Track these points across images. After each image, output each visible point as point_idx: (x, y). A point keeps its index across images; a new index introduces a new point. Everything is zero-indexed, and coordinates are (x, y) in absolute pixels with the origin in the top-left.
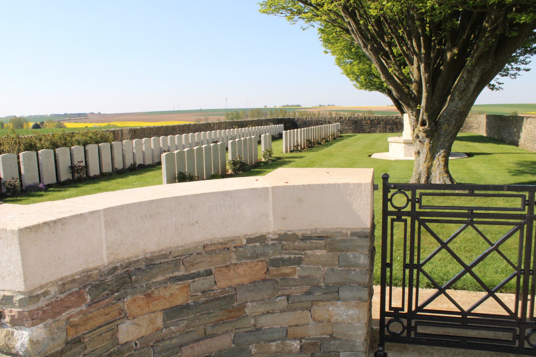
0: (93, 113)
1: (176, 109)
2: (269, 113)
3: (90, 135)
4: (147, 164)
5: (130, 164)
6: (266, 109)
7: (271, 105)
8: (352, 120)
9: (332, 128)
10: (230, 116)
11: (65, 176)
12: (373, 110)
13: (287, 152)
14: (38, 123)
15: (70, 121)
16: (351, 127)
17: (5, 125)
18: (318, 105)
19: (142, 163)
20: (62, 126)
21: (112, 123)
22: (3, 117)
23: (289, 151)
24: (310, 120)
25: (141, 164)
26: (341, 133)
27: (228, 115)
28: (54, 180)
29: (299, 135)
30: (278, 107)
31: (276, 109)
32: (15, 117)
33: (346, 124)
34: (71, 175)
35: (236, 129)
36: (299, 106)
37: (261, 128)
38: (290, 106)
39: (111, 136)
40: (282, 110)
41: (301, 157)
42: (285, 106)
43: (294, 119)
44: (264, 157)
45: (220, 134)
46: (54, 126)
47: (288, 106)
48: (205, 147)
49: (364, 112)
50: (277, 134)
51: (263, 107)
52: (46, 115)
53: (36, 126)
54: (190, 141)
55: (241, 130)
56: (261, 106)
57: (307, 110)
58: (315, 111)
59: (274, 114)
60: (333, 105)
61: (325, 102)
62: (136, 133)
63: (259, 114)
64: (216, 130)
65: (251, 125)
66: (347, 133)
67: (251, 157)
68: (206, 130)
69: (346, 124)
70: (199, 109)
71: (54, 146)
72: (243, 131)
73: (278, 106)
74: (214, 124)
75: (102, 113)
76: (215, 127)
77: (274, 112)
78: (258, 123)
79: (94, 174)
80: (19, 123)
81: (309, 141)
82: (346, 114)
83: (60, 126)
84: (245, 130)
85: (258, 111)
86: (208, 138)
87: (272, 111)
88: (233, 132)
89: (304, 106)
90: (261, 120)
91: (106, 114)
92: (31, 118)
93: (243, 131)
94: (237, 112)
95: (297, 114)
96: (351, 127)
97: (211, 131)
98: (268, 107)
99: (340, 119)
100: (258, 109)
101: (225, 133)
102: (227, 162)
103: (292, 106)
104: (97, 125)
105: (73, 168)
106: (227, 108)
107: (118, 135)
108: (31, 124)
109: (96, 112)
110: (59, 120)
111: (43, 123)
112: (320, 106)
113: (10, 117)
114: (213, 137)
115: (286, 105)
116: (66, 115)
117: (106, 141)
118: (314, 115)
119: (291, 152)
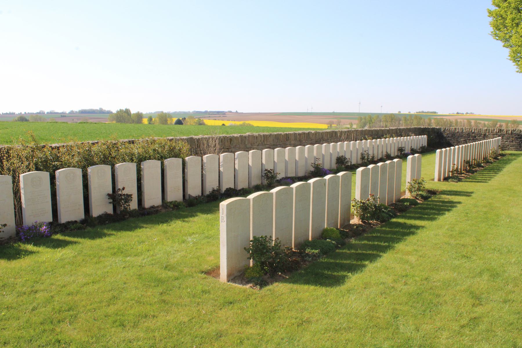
0: (231, 112)
1: (310, 111)
2: (403, 119)
3: (156, 146)
4: (239, 187)
5: (211, 190)
6: (400, 114)
7: (405, 110)
8: (516, 134)
9: (492, 144)
10: (363, 120)
11: (100, 207)
12: (518, 120)
13: (439, 180)
14: (181, 119)
15: (209, 118)
16: (514, 143)
17: (153, 119)
18: (456, 113)
19: (233, 187)
20: (201, 122)
21: (247, 122)
22: (153, 112)
23: (442, 178)
24: (460, 131)
25: (230, 189)
26: (503, 150)
27: (361, 119)
28: (79, 215)
29: (454, 155)
30: (412, 113)
31: (411, 116)
32: (162, 112)
33: (508, 139)
34: (111, 207)
35: (369, 141)
36: (435, 113)
37: (400, 139)
38: (425, 113)
39: (186, 148)
40: (418, 117)
41: (468, 194)
42: (420, 112)
43: (440, 129)
44: (411, 191)
45: (348, 146)
46: (194, 122)
47: (423, 112)
48: (314, 183)
49: (507, 122)
50: (418, 148)
51: (397, 113)
52: (189, 112)
53: (179, 122)
54: (306, 155)
55: (376, 142)
56: (395, 111)
57: (444, 117)
58: (452, 119)
59: (408, 120)
60: (472, 113)
61: (463, 110)
62: (230, 144)
63: (392, 119)
64: (343, 141)
65: (388, 136)
66: (508, 150)
67: (390, 192)
68: (328, 141)
69: (508, 139)
70: (332, 111)
71: (87, 162)
72: (378, 143)
73: (413, 112)
74: (341, 132)
75: (239, 111)
76: (343, 137)
77: (408, 118)
78: (397, 133)
79: (151, 205)
80: (164, 118)
81: (468, 162)
82: (486, 123)
83: (201, 124)
84: (380, 142)
85: (392, 118)
86: (331, 151)
87: (408, 117)
88: (366, 143)
89: (440, 113)
90: (400, 129)
91: (242, 113)
92: (176, 114)
93: (378, 143)
94: (369, 118)
95: (433, 121)
96: (514, 143)
97: (337, 142)
98: (402, 113)
99: (500, 133)
100: (392, 114)
101: (354, 145)
102: (353, 203)
103: (428, 112)
104: (233, 123)
105: (116, 197)
106: (361, 112)
107: (197, 147)
108: (175, 120)
109: (234, 111)
110: (199, 118)
111: (185, 119)
112: (458, 113)
113: (158, 112)
114: (338, 150)
115: (418, 111)
116: (206, 112)
117: (176, 156)
118: (447, 120)
119: (446, 179)
